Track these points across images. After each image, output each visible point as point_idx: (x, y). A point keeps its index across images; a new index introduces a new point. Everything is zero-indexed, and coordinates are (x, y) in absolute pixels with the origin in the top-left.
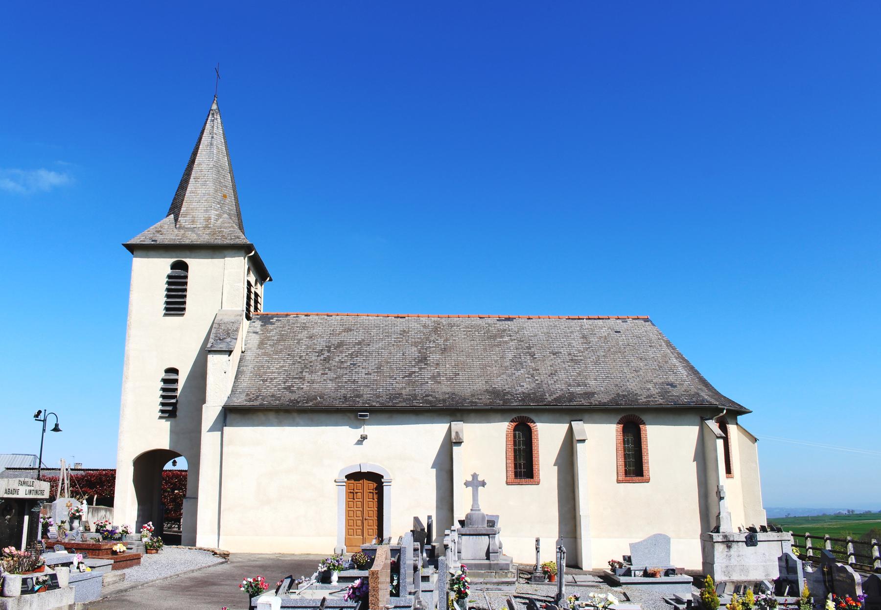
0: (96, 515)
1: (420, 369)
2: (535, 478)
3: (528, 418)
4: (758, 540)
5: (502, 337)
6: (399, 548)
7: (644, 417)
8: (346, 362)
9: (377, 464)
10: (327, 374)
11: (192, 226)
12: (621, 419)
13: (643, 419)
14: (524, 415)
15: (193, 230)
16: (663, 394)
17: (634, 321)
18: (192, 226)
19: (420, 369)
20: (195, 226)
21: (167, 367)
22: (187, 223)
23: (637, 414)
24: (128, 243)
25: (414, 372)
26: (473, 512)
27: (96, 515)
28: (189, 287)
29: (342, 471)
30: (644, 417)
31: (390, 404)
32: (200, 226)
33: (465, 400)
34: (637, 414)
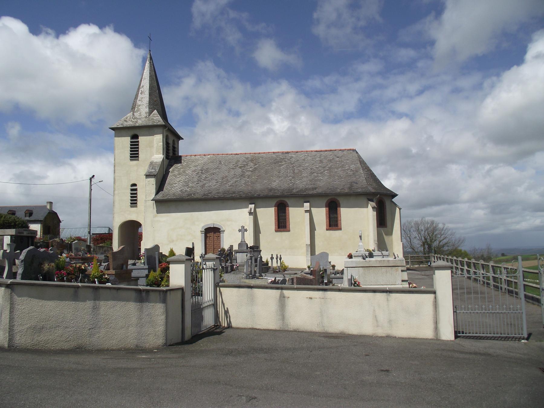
0: (101, 249)
1: (240, 179)
2: (288, 229)
3: (284, 201)
4: (374, 255)
5: (281, 162)
6: (106, 231)
7: (289, 201)
8: (208, 177)
9: (218, 223)
10: (199, 183)
11: (140, 117)
12: (276, 203)
13: (338, 200)
14: (282, 199)
15: (140, 119)
16: (350, 188)
17: (348, 151)
18: (140, 117)
19: (240, 179)
20: (141, 117)
21: (131, 184)
22: (138, 116)
23: (335, 198)
24: (112, 127)
25: (237, 181)
26: (241, 243)
27: (101, 249)
28: (129, 152)
29: (203, 227)
30: (289, 201)
31: (223, 196)
32: (143, 117)
33: (337, 188)
34: (336, 197)
